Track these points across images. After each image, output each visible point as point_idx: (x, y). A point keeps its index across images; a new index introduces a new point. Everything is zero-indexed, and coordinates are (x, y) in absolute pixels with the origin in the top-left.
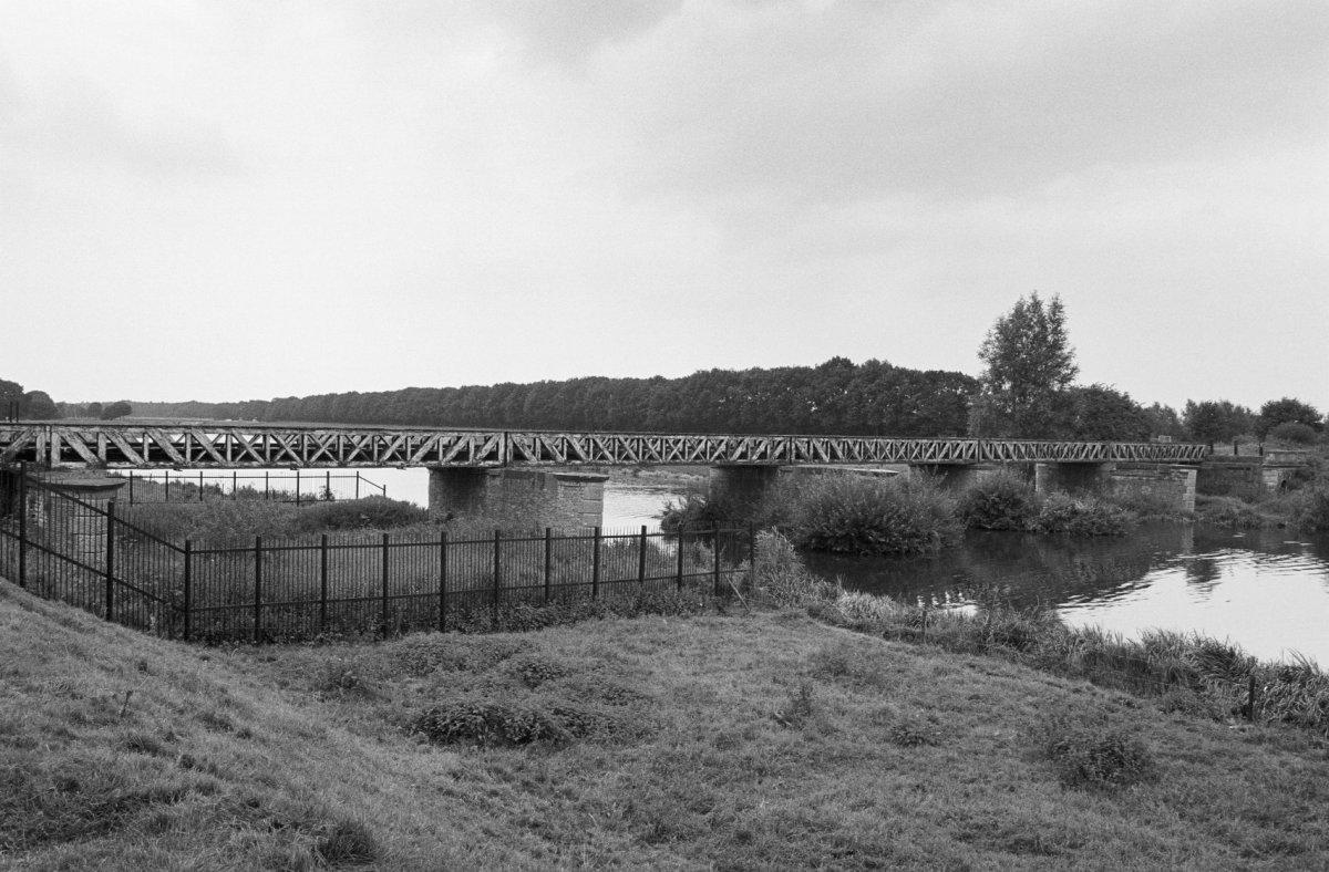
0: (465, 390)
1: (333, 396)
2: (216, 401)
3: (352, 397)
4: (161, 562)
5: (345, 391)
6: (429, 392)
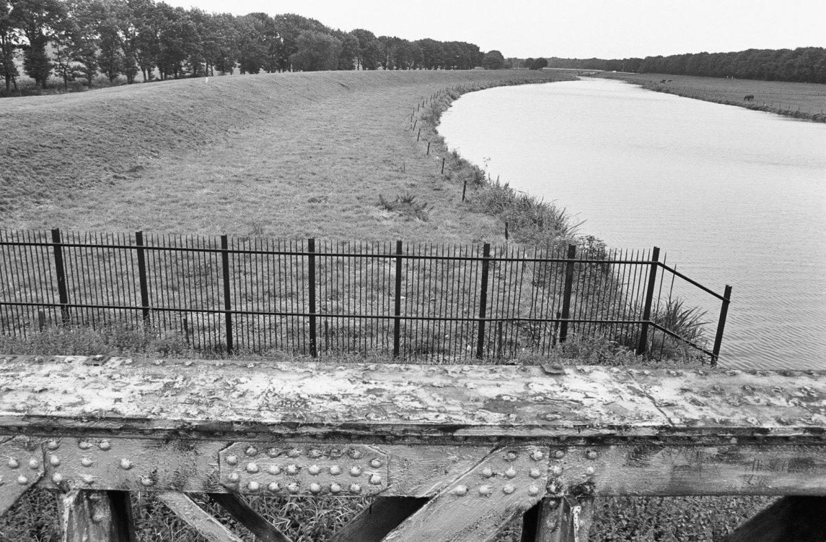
0: (800, 51)
1: (689, 55)
2: (609, 58)
3: (703, 56)
4: (273, 335)
5: (685, 53)
6: (768, 53)
